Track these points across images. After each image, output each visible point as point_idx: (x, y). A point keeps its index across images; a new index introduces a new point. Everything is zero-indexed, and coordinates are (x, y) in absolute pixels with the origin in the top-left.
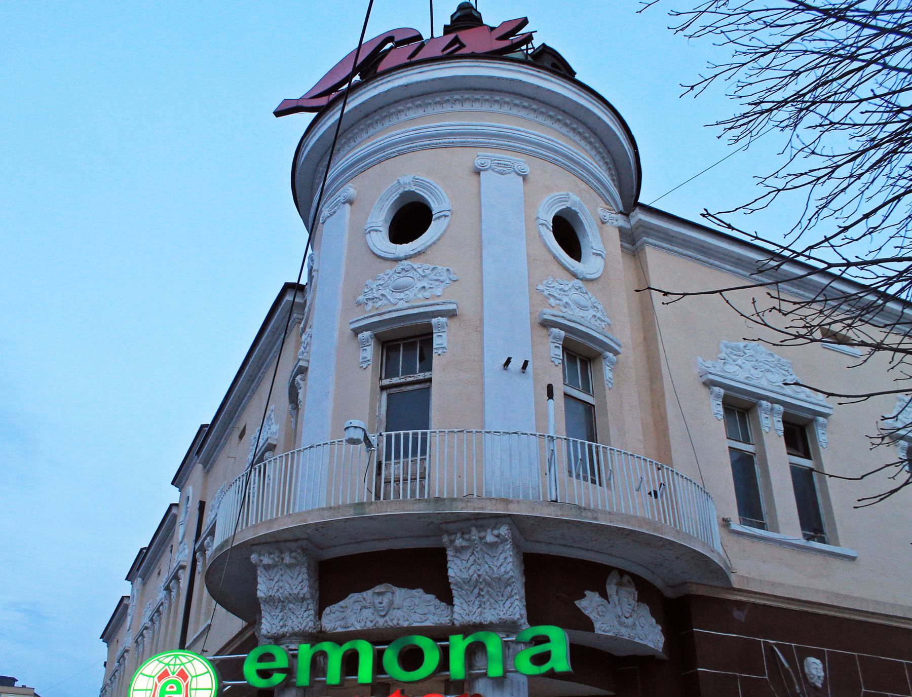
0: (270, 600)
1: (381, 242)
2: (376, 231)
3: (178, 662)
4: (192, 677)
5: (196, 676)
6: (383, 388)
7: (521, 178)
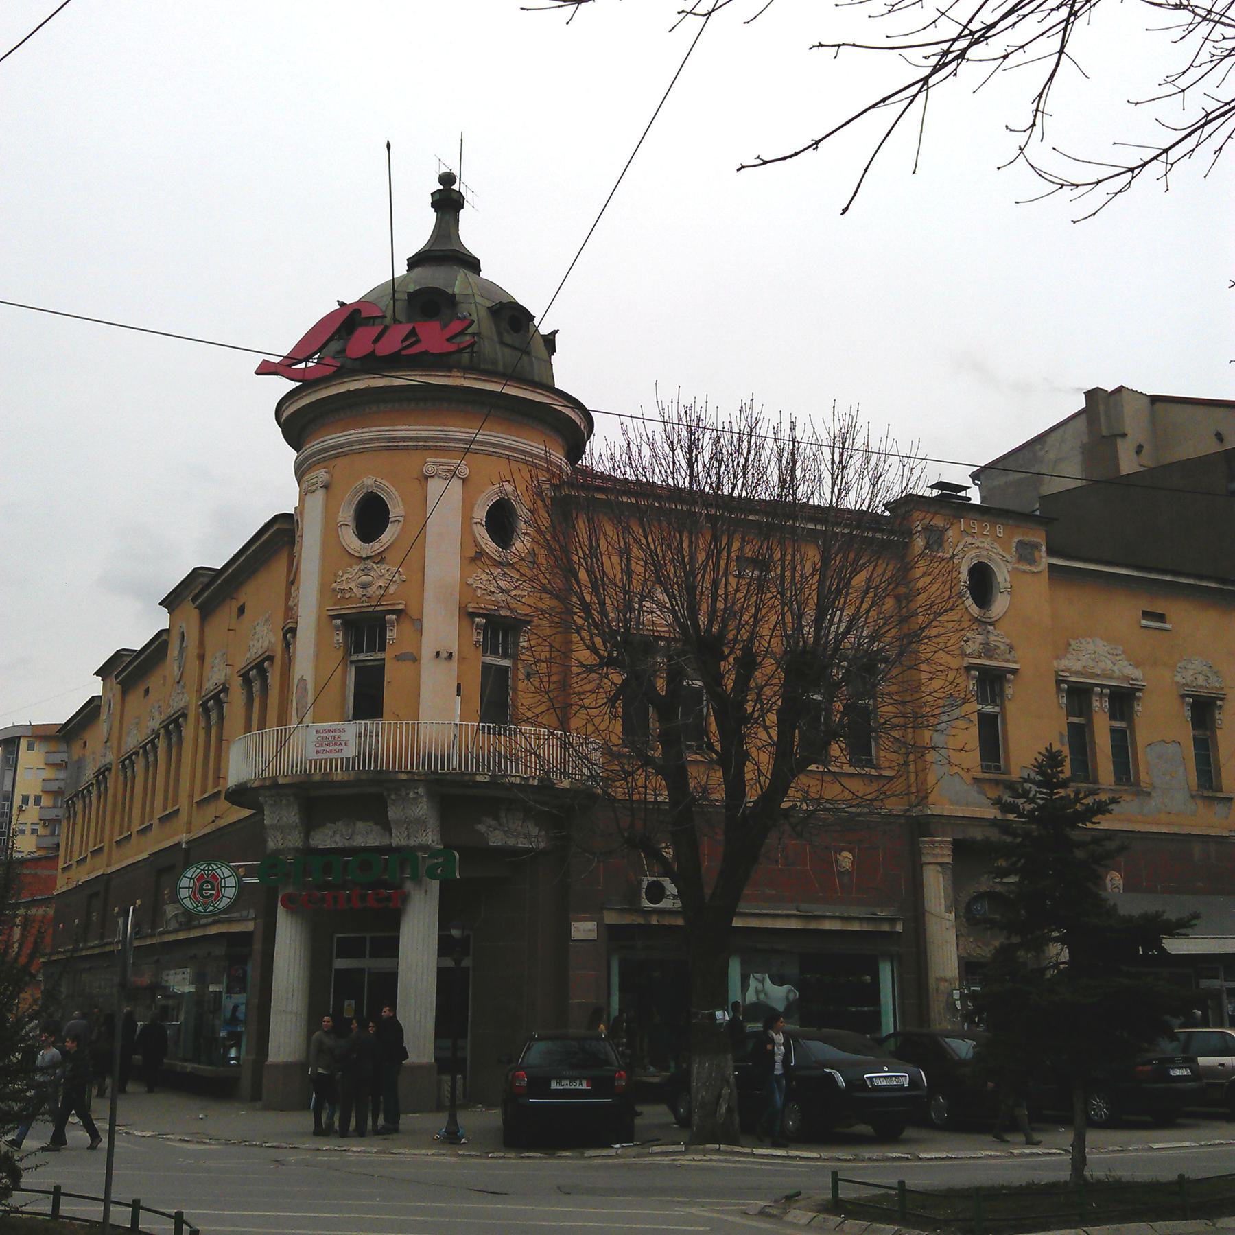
0: (273, 827)
1: (352, 541)
2: (346, 525)
3: (210, 868)
4: (222, 879)
5: (224, 878)
6: (352, 662)
7: (462, 481)
